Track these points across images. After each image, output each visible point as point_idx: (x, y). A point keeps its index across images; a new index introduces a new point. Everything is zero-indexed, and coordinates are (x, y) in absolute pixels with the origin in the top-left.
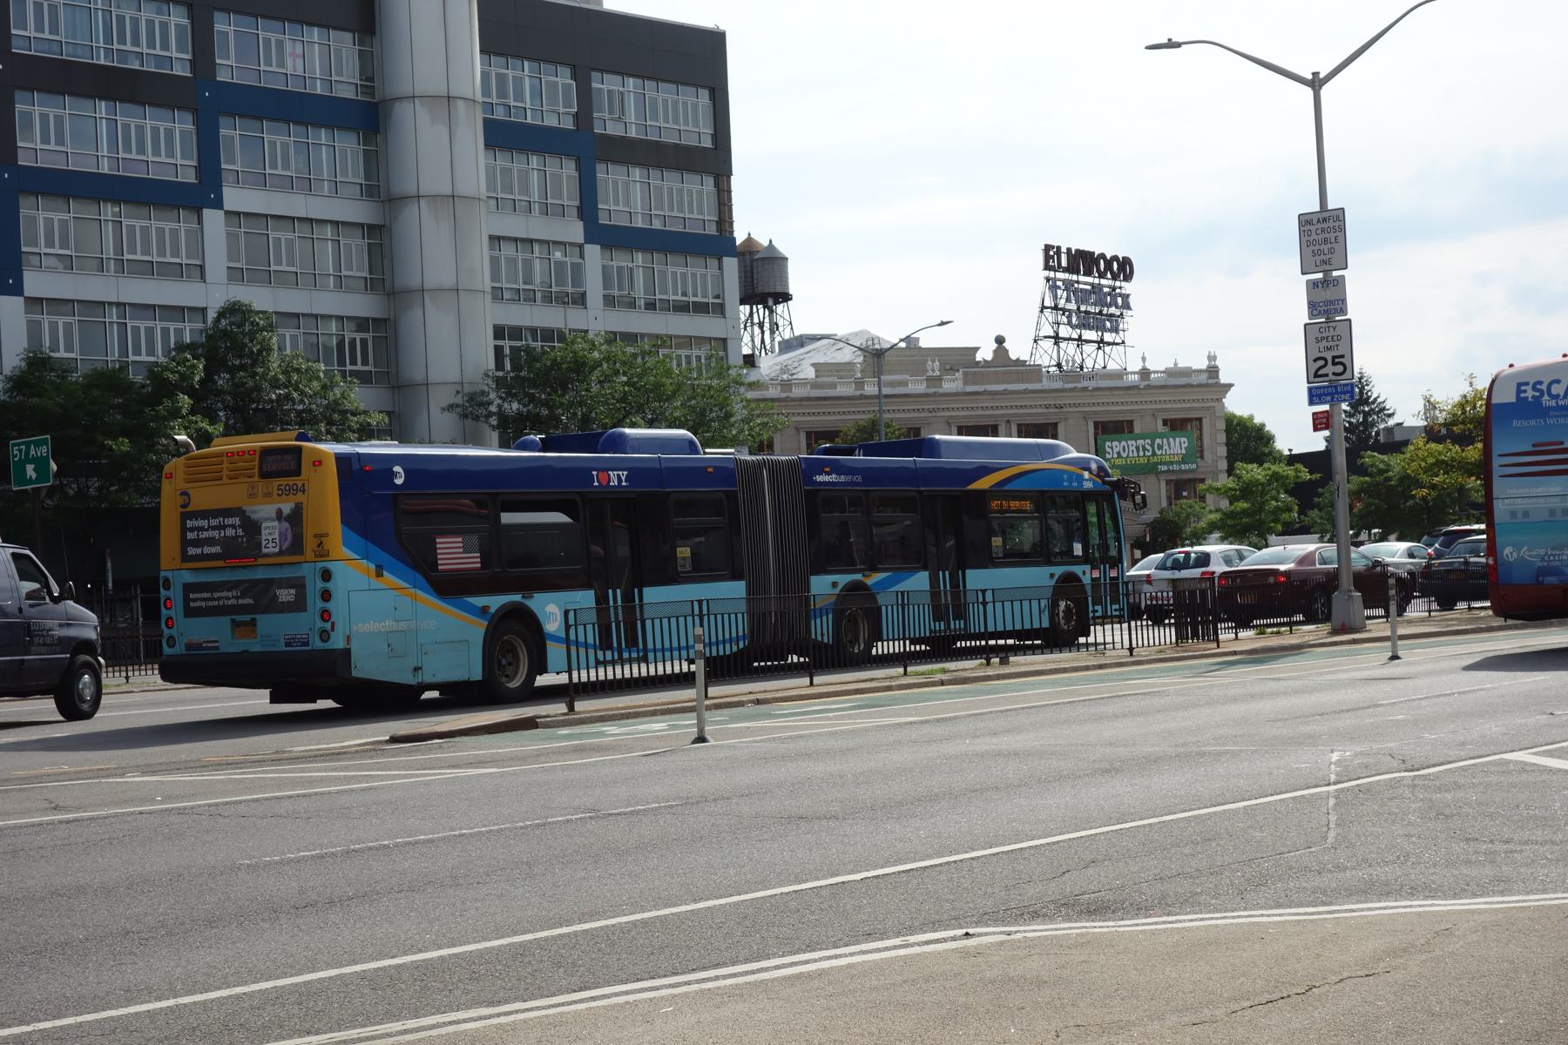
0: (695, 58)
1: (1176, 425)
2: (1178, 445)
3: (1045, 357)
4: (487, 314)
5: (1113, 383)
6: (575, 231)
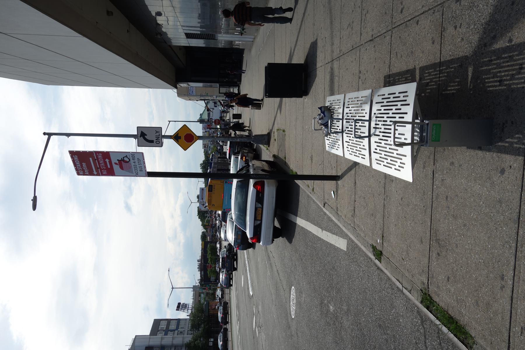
0: (157, 323)
1: (200, 296)
2: (202, 295)
3: (190, 311)
4: (186, 335)
5: (194, 302)
6: (176, 331)
